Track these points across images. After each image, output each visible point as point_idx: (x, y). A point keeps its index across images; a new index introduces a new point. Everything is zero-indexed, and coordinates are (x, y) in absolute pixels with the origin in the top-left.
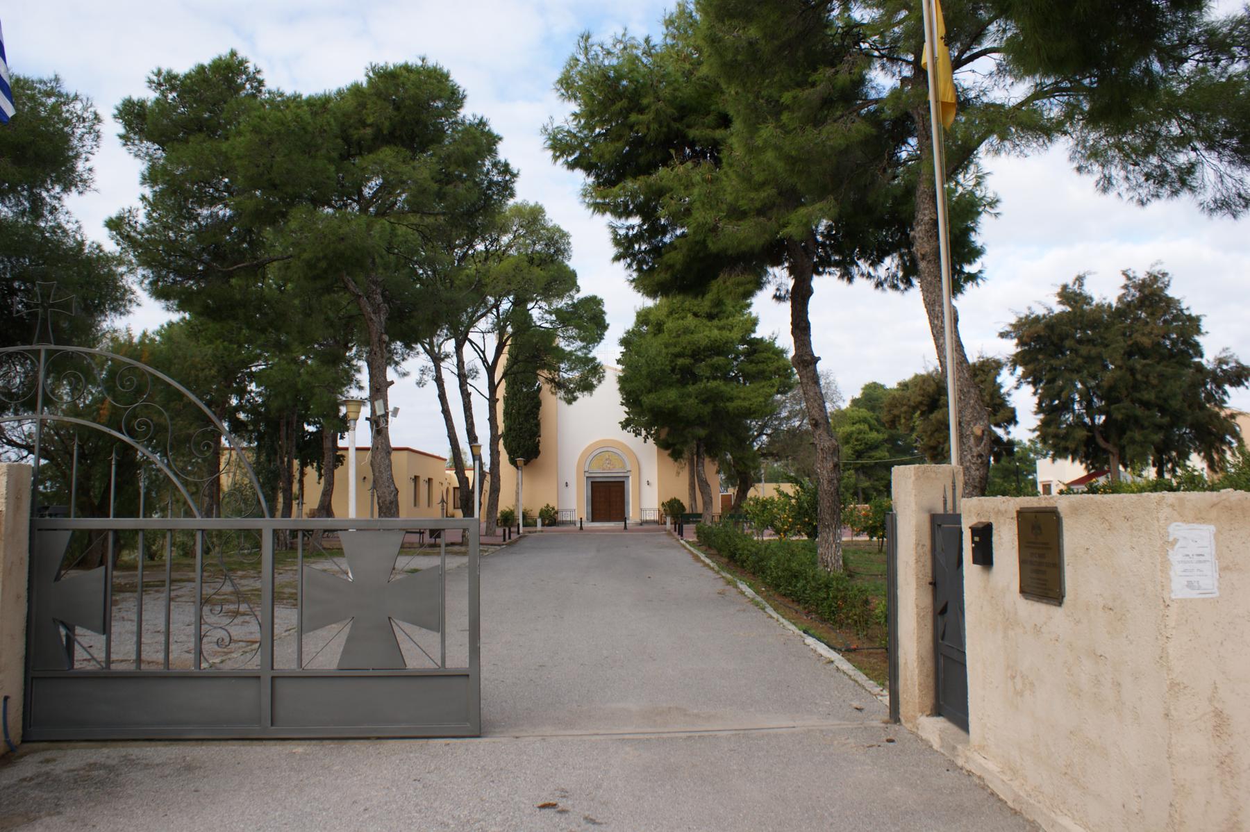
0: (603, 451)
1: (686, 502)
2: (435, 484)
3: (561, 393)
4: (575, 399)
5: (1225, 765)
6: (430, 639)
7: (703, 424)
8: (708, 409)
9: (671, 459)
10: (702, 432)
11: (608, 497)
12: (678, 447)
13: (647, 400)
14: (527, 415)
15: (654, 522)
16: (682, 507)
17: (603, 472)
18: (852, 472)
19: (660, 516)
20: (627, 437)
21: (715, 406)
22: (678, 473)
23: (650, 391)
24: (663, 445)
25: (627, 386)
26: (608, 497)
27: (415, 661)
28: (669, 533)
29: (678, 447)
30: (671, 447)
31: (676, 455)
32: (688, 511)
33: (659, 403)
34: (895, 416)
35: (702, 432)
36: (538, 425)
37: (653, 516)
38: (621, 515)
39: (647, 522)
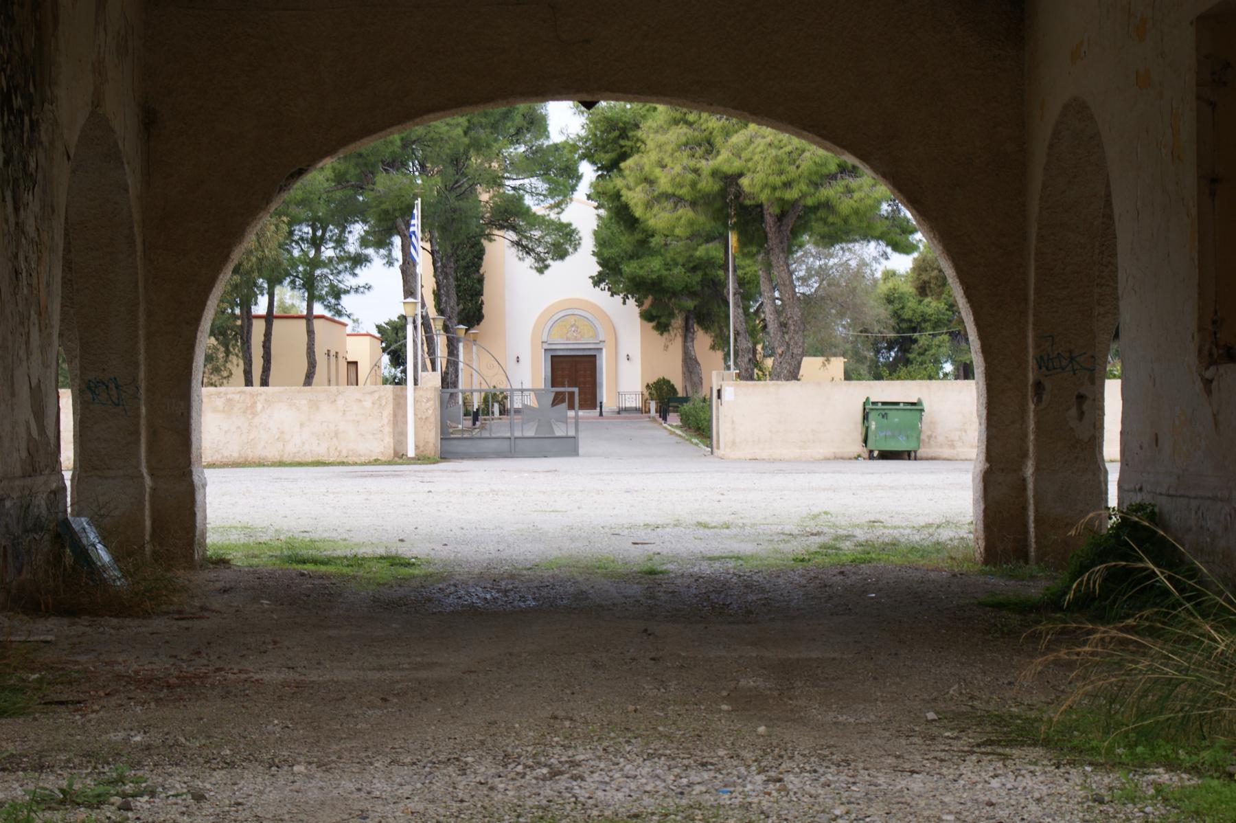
0: (568, 314)
1: (678, 382)
2: (340, 356)
3: (530, 260)
4: (547, 267)
5: (734, 429)
6: (563, 426)
7: (692, 294)
8: (698, 276)
9: (656, 333)
10: (690, 304)
11: (574, 375)
12: (663, 320)
13: (629, 268)
14: (467, 267)
15: (636, 410)
16: (672, 389)
17: (567, 343)
18: (946, 337)
19: (645, 402)
20: (601, 298)
21: (706, 274)
22: (666, 347)
23: (631, 257)
24: (647, 316)
25: (606, 254)
26: (574, 375)
27: (558, 434)
28: (654, 420)
29: (663, 320)
30: (657, 318)
31: (662, 328)
32: (681, 394)
33: (641, 272)
34: (925, 282)
35: (690, 304)
36: (481, 280)
37: (634, 402)
38: (590, 400)
39: (626, 410)
